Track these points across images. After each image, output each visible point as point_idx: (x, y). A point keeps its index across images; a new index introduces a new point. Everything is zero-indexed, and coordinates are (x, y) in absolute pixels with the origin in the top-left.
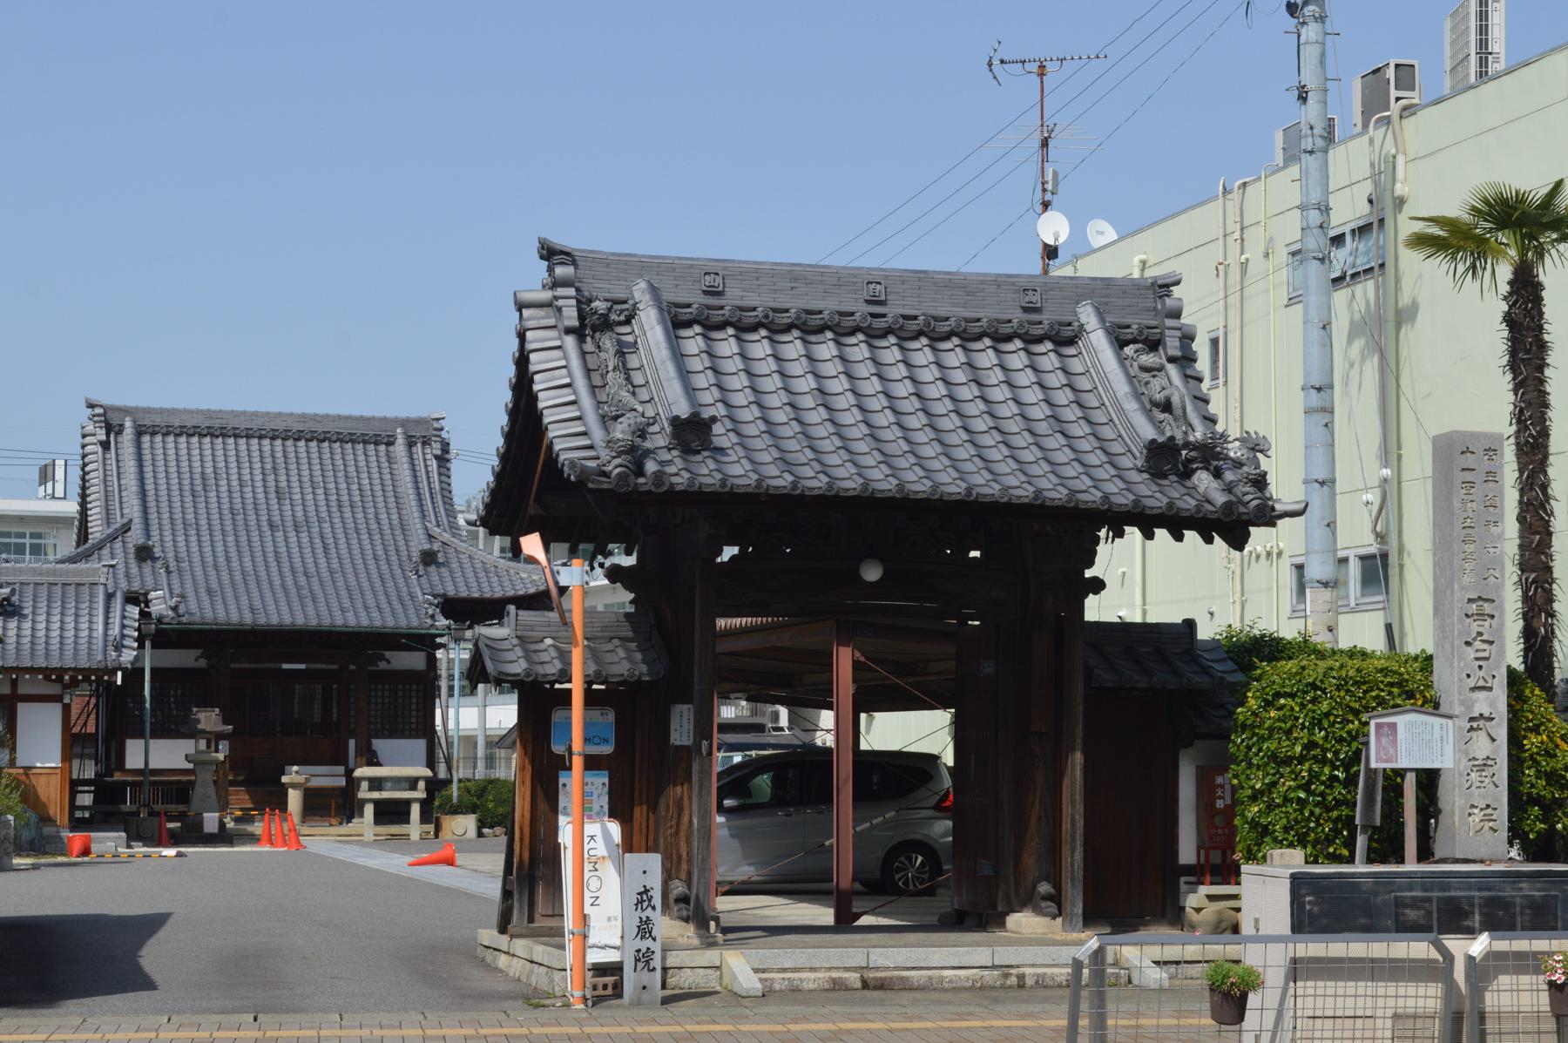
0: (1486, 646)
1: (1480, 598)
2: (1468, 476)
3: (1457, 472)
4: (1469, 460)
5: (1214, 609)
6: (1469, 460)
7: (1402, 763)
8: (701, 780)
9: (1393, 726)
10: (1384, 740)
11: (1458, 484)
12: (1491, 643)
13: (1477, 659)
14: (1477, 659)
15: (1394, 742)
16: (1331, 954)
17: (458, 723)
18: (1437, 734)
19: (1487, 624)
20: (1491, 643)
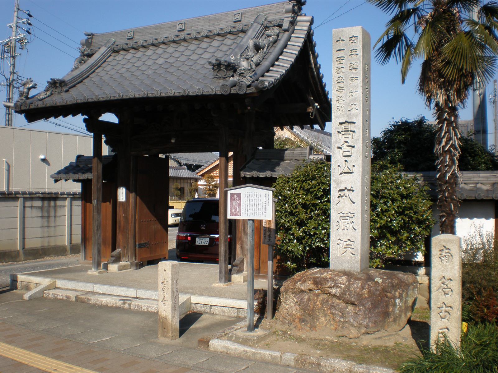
0: (349, 149)
1: (346, 122)
2: (341, 54)
3: (334, 52)
4: (341, 45)
5: (42, 157)
6: (341, 45)
7: (244, 216)
8: (55, 267)
9: (239, 195)
10: (234, 203)
11: (335, 59)
12: (353, 147)
13: (344, 156)
14: (344, 156)
15: (240, 205)
16: (92, 285)
17: (24, 239)
18: (263, 200)
19: (350, 136)
20: (353, 147)
